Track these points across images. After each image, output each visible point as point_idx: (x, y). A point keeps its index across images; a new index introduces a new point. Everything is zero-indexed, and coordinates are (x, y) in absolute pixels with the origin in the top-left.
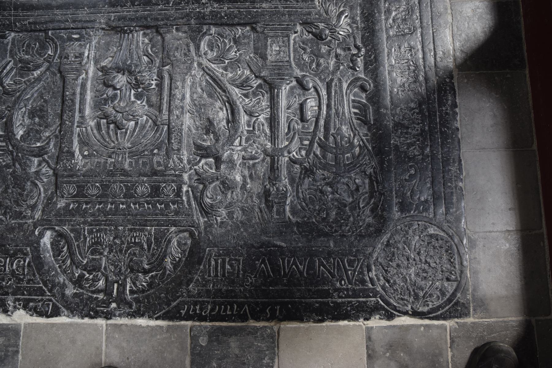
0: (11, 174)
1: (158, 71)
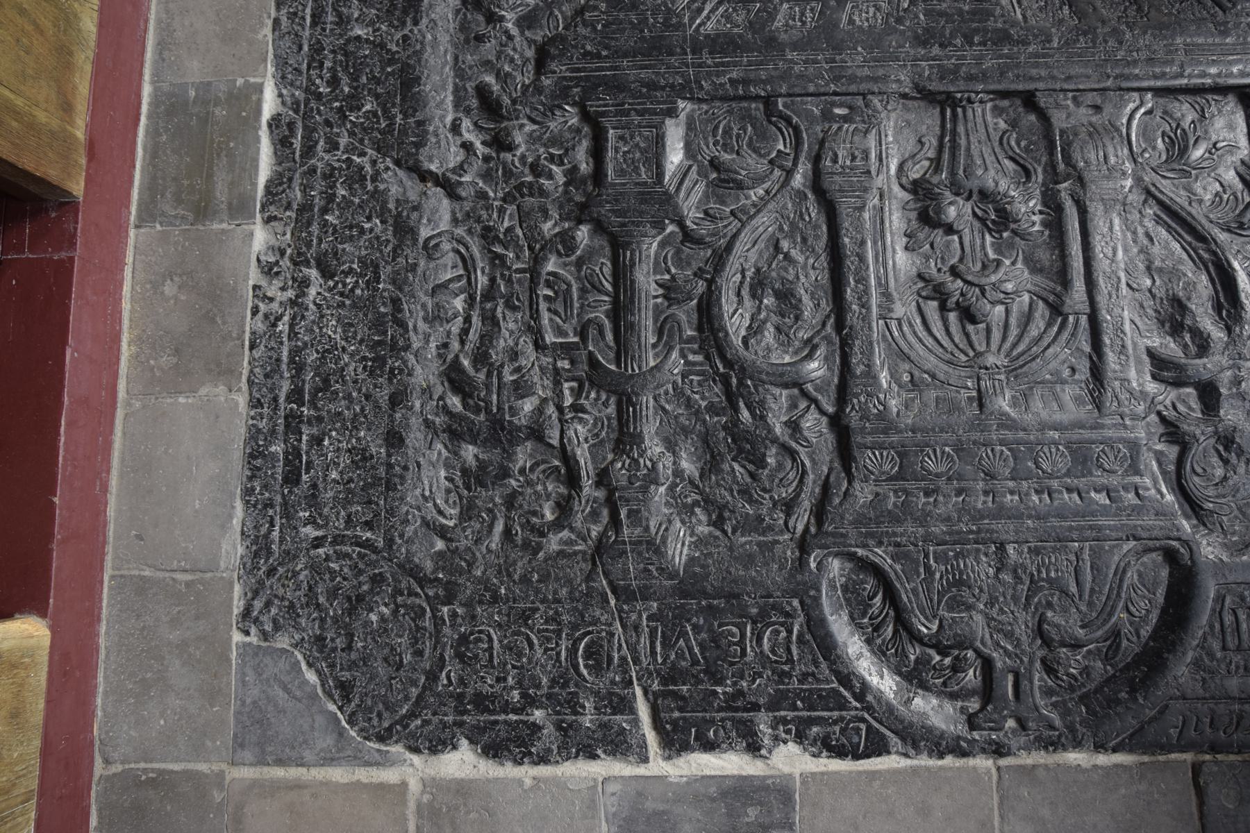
0: (725, 428)
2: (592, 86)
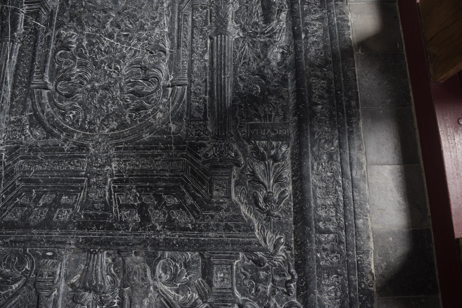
1: (120, 291)
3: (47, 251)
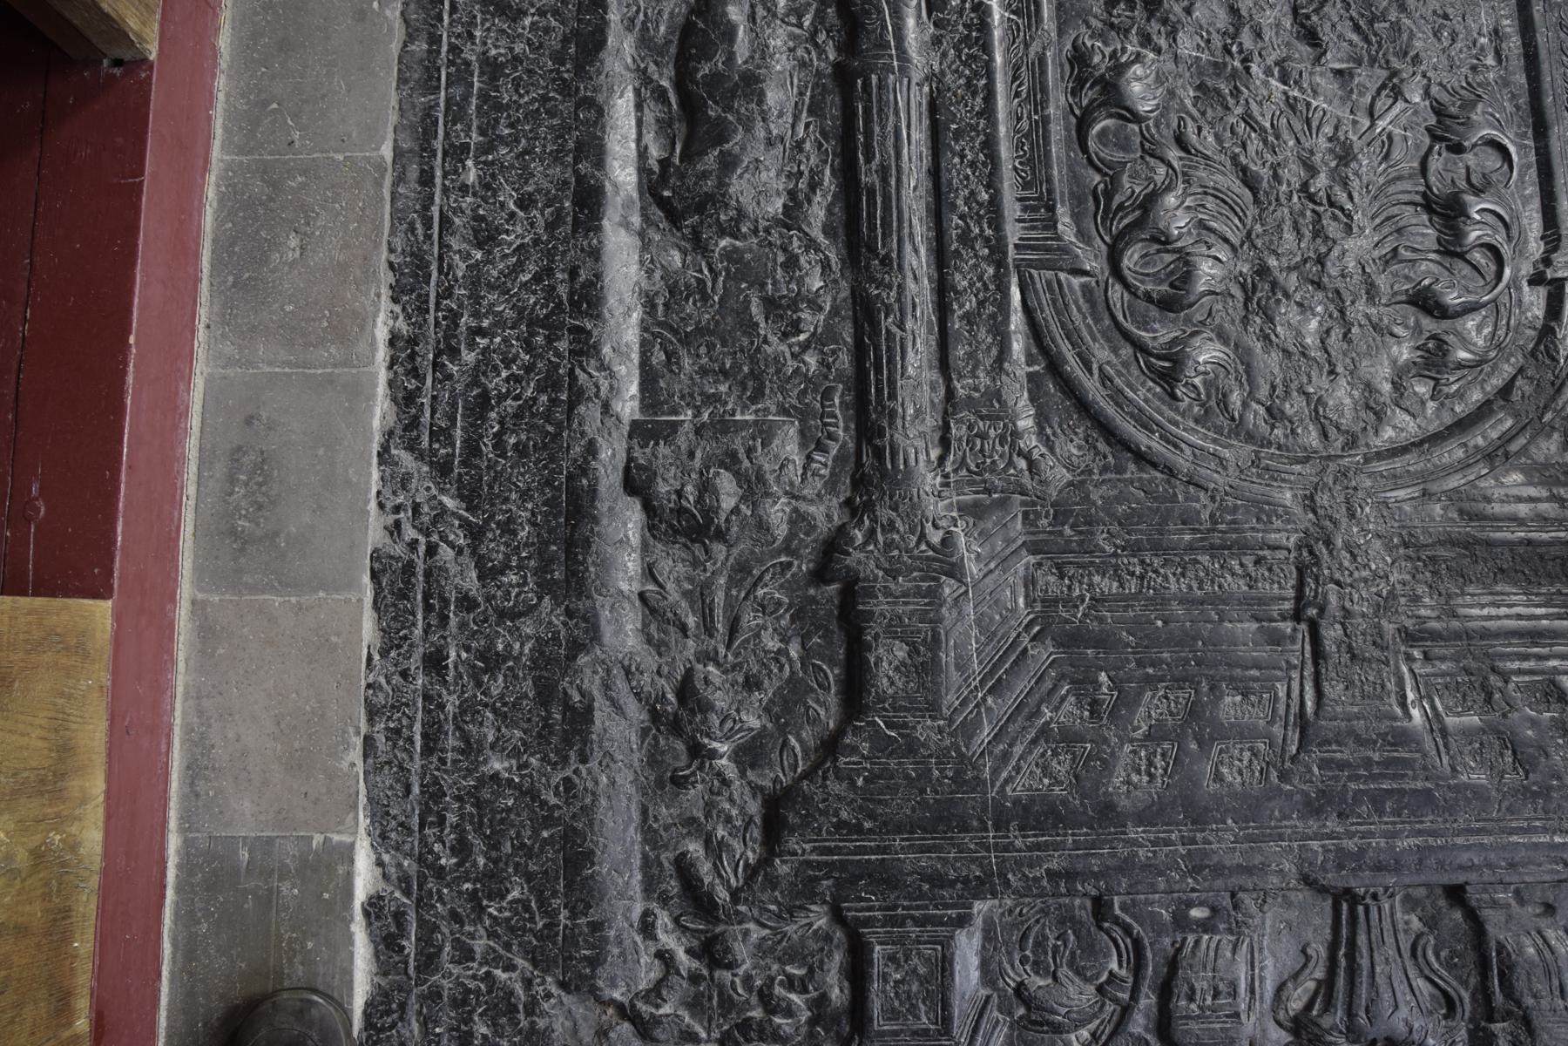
2: (849, 878)
3: (1190, 904)
